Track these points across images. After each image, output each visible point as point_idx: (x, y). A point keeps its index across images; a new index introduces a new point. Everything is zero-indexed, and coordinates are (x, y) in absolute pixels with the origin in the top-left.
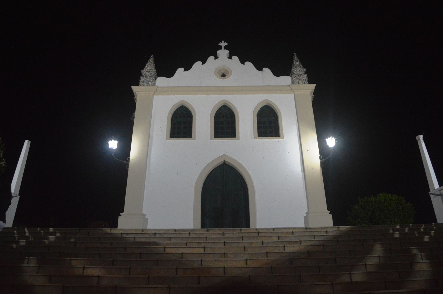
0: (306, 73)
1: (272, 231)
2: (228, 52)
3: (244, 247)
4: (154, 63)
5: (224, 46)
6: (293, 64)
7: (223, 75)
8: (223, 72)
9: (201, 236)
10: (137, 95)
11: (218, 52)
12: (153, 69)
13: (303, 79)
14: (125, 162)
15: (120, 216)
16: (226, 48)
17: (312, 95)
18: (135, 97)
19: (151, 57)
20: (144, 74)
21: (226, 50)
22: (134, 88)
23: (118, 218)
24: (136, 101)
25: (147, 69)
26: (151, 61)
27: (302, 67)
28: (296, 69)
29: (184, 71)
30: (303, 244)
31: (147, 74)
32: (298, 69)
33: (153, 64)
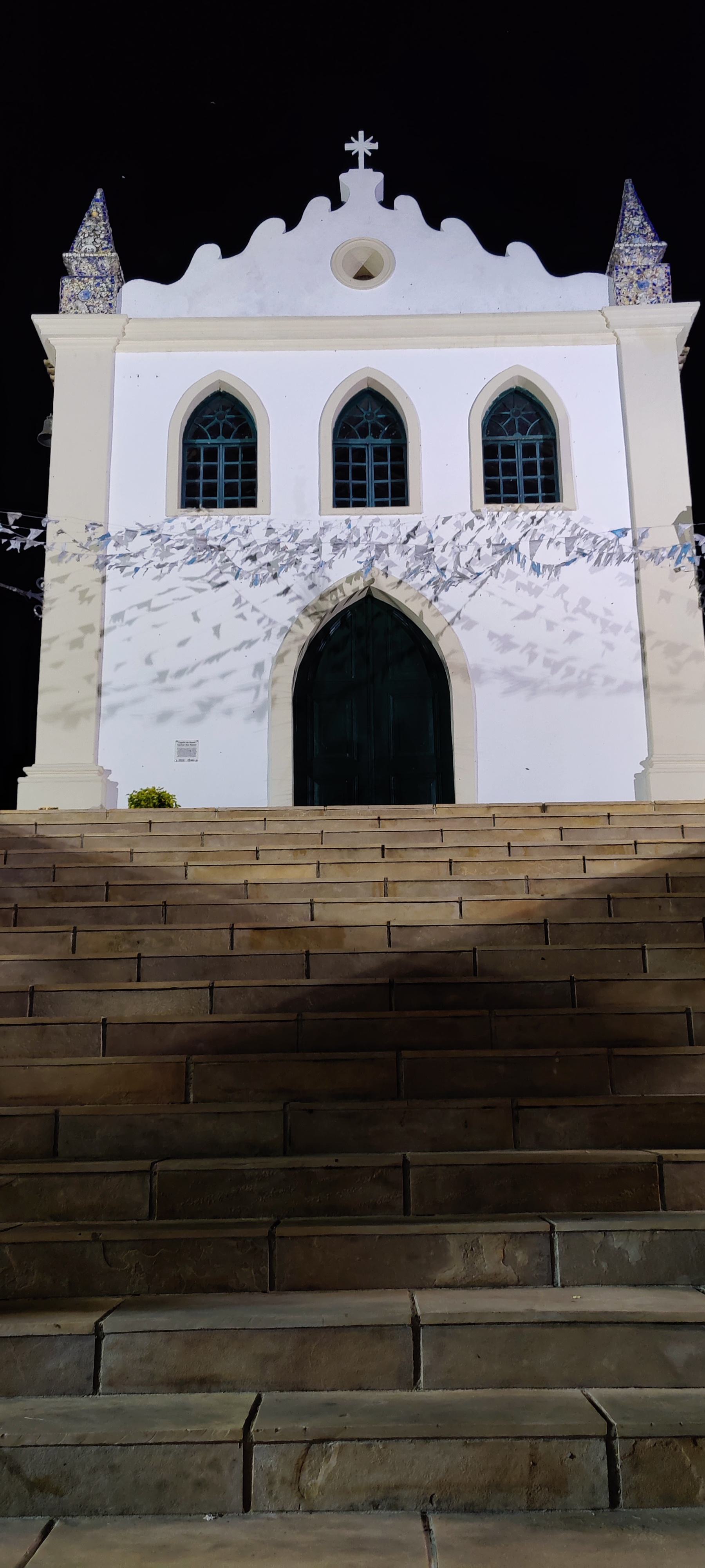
0: (665, 259)
1: (537, 812)
2: (380, 176)
3: (450, 862)
4: (110, 222)
5: (365, 155)
6: (620, 225)
7: (364, 275)
8: (362, 259)
9: (304, 830)
10: (52, 347)
11: (343, 178)
12: (106, 248)
13: (654, 285)
14: (30, 595)
15: (24, 775)
16: (372, 162)
17: (682, 348)
18: (47, 358)
19: (97, 201)
20: (73, 268)
21: (374, 170)
22: (42, 322)
23: (17, 783)
24: (54, 374)
25: (83, 249)
26: (94, 214)
27: (653, 234)
28: (631, 245)
29: (219, 259)
30: (645, 852)
31: (87, 268)
32: (639, 245)
33: (103, 228)
